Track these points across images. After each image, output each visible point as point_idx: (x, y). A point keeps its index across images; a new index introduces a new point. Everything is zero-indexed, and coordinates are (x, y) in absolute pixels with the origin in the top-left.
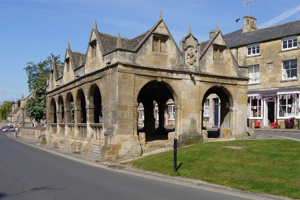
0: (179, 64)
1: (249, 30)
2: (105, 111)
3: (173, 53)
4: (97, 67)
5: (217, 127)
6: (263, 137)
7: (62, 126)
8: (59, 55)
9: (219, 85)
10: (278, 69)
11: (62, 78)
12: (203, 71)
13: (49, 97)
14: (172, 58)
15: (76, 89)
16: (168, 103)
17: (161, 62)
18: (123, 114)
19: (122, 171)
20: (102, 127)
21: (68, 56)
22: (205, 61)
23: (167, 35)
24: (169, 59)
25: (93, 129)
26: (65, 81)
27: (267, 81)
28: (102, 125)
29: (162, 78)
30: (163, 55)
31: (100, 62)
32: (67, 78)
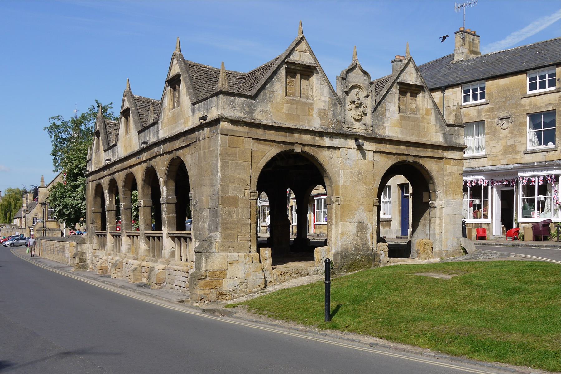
0: (335, 120)
3: (323, 99)
5: (406, 238)
7: (116, 236)
8: (111, 103)
9: (410, 160)
11: (115, 145)
12: (380, 133)
13: (93, 181)
14: (322, 108)
15: (142, 167)
16: (313, 192)
18: (230, 214)
19: (228, 320)
20: (190, 238)
21: (127, 105)
22: (383, 113)
23: (313, 65)
24: (315, 111)
26: (121, 152)
27: (500, 151)
28: (190, 234)
29: (304, 145)
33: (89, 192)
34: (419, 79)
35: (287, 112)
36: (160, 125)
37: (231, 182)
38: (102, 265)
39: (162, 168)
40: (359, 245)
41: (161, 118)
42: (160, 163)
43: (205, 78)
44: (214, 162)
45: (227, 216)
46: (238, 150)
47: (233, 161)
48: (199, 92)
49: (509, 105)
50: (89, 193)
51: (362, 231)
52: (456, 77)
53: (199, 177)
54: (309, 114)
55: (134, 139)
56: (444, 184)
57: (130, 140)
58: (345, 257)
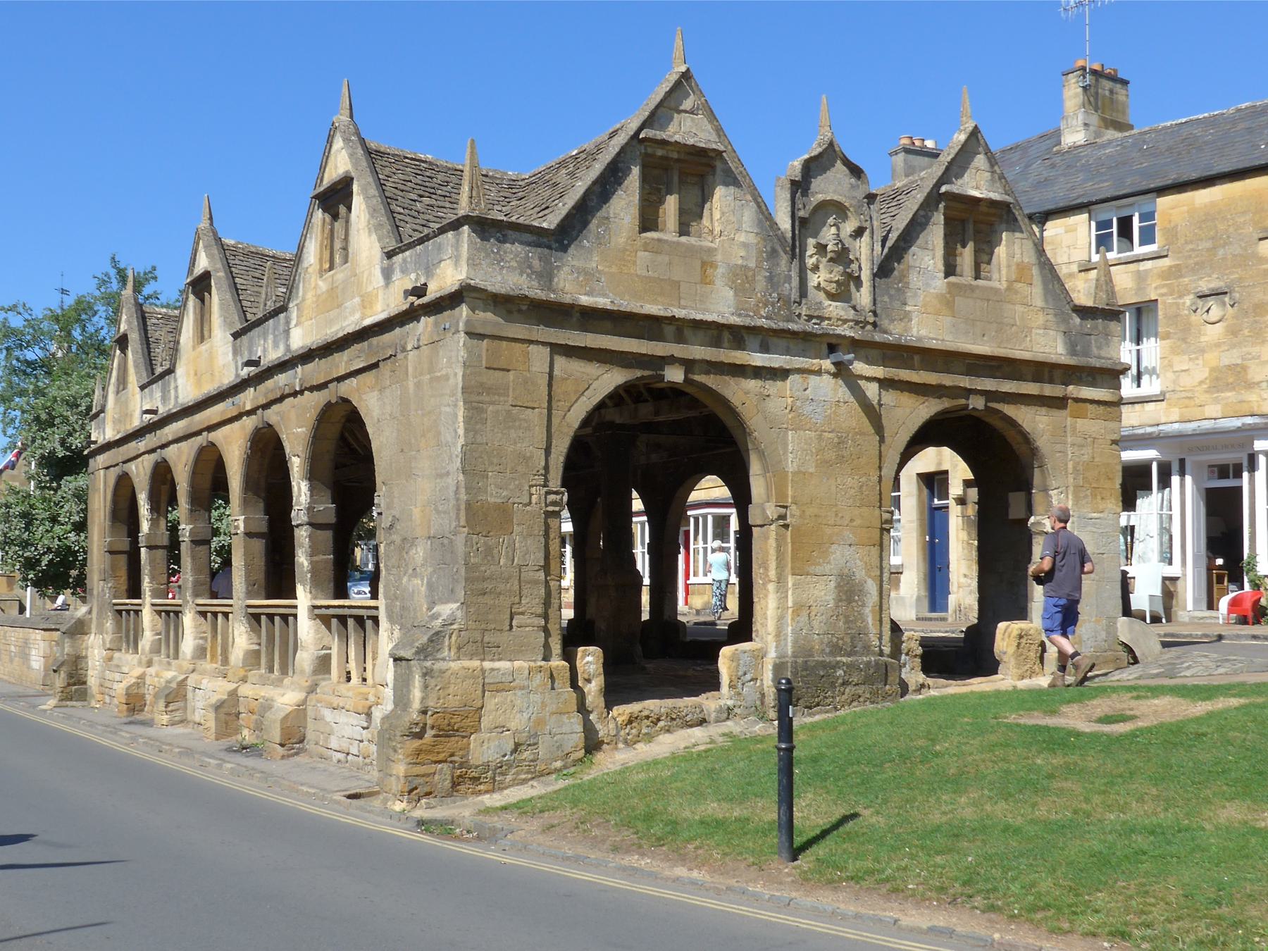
0: (775, 295)
1: (1095, 132)
2: (394, 537)
3: (741, 238)
4: (352, 313)
5: (944, 619)
6: (1221, 670)
7: (168, 613)
8: (154, 268)
9: (977, 403)
10: (1256, 322)
11: (170, 371)
12: (895, 332)
13: (107, 468)
14: (740, 262)
15: (243, 428)
16: (694, 496)
17: (683, 286)
19: (492, 854)
20: (375, 620)
21: (203, 263)
22: (903, 277)
23: (714, 146)
24: (721, 270)
25: (330, 631)
26: (186, 388)
27: (1201, 382)
28: (376, 608)
30: (692, 251)
31: (370, 289)
32: (196, 374)
33: (97, 496)
34: (998, 185)
35: (644, 273)
36: (294, 313)
37: (492, 463)
38: (130, 692)
39: (299, 430)
40: (842, 639)
41: (297, 297)
42: (293, 415)
43: (418, 187)
44: (448, 409)
45: (483, 560)
46: (511, 375)
47: (499, 407)
48: (402, 224)
49: (1224, 259)
50: (97, 500)
51: (850, 600)
52: (1073, 188)
53: (402, 451)
54: (706, 280)
55: (220, 353)
56: (1070, 471)
57: (211, 357)
58: (804, 673)
